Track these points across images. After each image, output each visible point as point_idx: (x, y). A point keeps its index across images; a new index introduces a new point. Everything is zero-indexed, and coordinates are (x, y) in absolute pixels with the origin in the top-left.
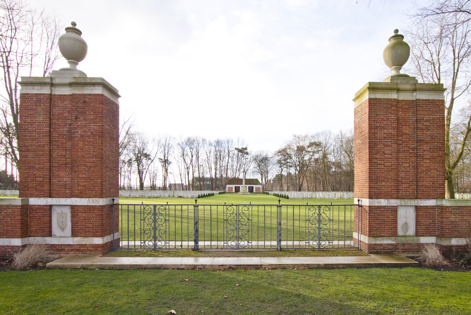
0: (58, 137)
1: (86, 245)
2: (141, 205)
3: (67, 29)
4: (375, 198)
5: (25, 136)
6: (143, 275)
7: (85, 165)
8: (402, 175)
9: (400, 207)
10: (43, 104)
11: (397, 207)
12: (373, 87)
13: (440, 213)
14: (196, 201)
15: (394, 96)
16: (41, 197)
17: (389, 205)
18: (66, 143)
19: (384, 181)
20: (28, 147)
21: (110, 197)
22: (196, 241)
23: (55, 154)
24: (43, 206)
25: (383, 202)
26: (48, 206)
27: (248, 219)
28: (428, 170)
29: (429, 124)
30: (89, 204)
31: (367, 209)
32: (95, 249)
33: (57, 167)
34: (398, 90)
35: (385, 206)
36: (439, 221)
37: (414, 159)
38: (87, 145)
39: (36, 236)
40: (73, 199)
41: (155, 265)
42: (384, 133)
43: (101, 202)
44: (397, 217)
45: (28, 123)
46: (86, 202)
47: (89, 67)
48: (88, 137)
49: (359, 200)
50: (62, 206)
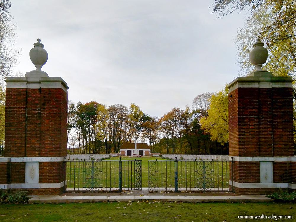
0: (31, 116)
1: (48, 188)
2: (135, 161)
3: (35, 44)
4: (243, 156)
5: (9, 116)
6: (86, 209)
7: (49, 135)
8: (263, 140)
9: (261, 162)
10: (22, 94)
11: (259, 162)
12: (240, 81)
13: (290, 166)
14: (120, 158)
15: (256, 86)
16: (19, 157)
17: (254, 161)
18: (36, 121)
19: (250, 144)
20: (11, 123)
21: (63, 156)
22: (176, 186)
23: (29, 128)
24: (20, 162)
25: (249, 159)
26: (24, 162)
27: (212, 171)
28: (281, 136)
29: (281, 105)
30: (52, 161)
31: (238, 163)
32: (54, 191)
33: (30, 136)
34: (259, 82)
35: (251, 162)
36: (289, 172)
37: (271, 129)
38: (50, 122)
39: (15, 183)
40: (41, 158)
41: (124, 199)
42: (250, 112)
43: (58, 159)
44: (259, 169)
45: (11, 107)
46: (49, 159)
47: (51, 70)
48: (52, 116)
49: (232, 158)
50: (33, 164)
